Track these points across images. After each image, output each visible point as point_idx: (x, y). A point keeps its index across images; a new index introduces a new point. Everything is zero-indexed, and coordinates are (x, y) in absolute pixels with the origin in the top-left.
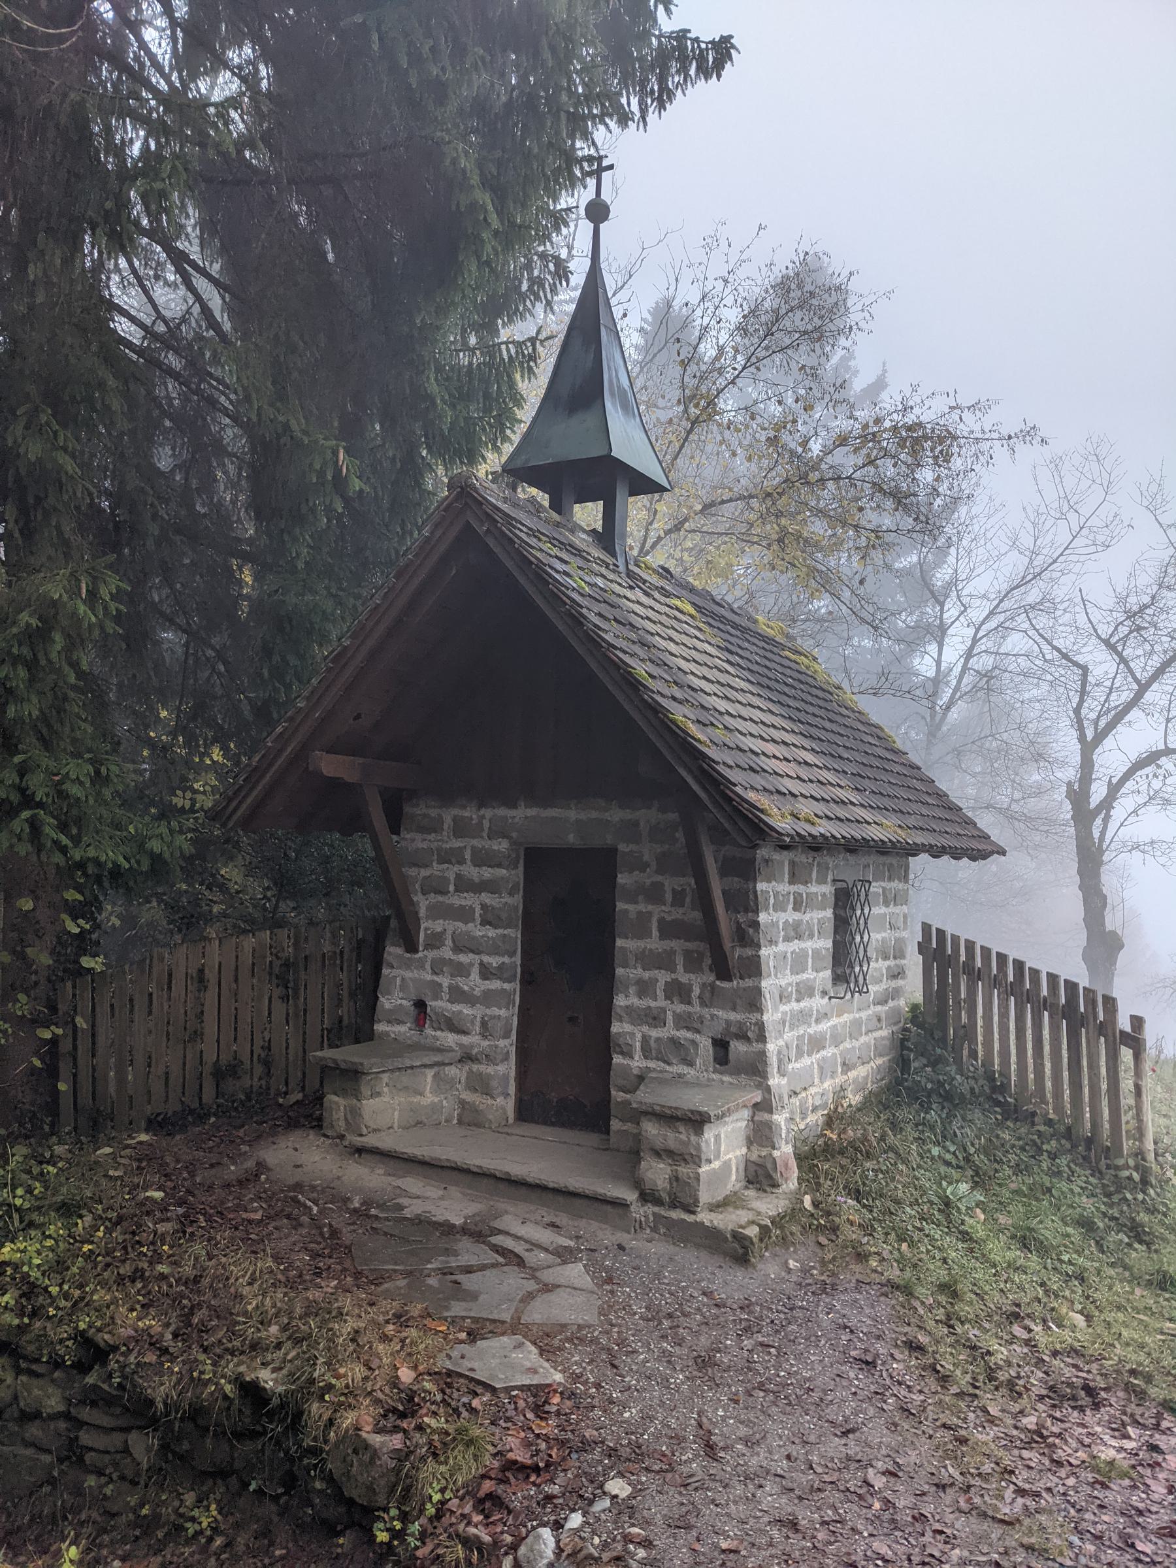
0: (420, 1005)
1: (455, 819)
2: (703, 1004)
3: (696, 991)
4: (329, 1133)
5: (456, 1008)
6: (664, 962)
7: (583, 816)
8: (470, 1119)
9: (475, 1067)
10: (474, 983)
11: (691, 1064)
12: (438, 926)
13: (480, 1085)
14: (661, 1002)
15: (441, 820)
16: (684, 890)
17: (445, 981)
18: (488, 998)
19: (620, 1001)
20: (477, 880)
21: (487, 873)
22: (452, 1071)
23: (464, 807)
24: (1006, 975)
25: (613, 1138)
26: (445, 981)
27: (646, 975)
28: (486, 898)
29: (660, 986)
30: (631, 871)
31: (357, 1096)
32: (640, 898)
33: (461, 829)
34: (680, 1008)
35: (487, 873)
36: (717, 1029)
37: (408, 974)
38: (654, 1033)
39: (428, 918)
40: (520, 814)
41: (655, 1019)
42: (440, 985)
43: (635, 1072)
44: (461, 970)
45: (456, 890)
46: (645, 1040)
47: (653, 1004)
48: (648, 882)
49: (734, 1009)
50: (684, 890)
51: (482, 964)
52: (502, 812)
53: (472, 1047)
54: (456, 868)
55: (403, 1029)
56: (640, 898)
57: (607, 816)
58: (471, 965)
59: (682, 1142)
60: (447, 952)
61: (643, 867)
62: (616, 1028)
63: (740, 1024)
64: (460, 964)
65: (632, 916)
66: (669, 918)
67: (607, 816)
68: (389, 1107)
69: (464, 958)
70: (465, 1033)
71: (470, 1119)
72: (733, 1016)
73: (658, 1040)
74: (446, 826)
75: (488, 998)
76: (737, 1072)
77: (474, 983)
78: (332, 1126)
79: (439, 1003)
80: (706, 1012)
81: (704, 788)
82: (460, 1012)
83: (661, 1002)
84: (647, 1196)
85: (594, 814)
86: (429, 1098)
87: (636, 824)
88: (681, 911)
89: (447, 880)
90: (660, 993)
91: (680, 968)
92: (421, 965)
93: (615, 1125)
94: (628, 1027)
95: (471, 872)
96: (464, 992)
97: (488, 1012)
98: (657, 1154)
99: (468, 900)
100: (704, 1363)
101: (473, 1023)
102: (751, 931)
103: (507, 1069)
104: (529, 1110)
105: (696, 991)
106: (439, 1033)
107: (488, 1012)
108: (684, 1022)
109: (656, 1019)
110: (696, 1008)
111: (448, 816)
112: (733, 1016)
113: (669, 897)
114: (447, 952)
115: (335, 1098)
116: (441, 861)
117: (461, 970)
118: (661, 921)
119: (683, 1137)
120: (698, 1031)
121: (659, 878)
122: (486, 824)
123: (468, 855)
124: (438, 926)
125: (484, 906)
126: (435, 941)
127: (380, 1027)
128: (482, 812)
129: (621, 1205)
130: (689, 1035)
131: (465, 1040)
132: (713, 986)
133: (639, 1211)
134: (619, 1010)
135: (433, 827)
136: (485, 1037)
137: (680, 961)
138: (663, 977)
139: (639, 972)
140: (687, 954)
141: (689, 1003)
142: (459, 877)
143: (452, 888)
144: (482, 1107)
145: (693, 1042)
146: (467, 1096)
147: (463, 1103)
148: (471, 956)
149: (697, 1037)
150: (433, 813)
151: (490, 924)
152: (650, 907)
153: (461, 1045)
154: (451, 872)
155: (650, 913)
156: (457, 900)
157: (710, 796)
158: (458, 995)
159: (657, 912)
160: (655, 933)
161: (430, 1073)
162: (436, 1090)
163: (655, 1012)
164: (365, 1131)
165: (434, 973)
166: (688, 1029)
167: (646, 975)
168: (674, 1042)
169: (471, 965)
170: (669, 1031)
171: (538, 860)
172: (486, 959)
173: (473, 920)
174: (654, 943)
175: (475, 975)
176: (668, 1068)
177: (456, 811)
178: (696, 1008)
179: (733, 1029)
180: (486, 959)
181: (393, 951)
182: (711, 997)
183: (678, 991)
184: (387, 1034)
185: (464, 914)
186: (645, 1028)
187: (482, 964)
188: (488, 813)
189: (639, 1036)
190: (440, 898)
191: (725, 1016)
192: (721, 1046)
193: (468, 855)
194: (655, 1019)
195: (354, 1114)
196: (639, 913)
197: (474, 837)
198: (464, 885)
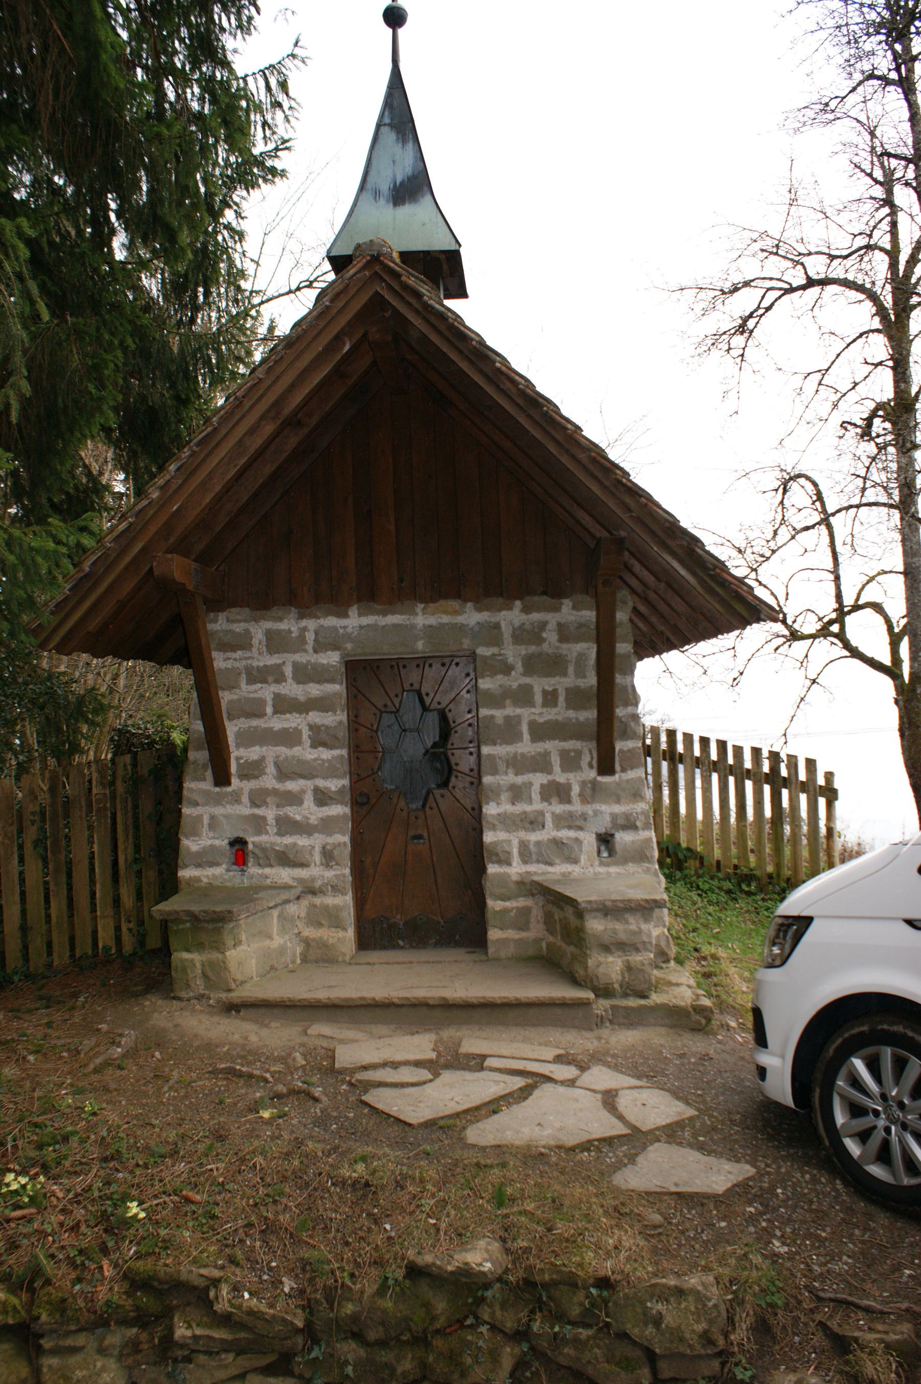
0: (239, 844)
1: (269, 634)
2: (584, 799)
3: (576, 790)
4: (183, 994)
5: (288, 840)
6: (541, 764)
7: (432, 620)
8: (317, 956)
9: (318, 901)
10: (310, 811)
11: (576, 861)
12: (254, 753)
13: (316, 918)
14: (537, 805)
15: (247, 634)
16: (555, 690)
17: (270, 813)
18: (326, 826)
19: (490, 810)
20: (302, 699)
21: (314, 690)
22: (292, 909)
23: (280, 619)
24: (654, 763)
25: (491, 950)
26: (270, 813)
27: (519, 780)
28: (315, 717)
29: (536, 788)
30: (493, 675)
31: (219, 947)
32: (508, 702)
33: (275, 643)
34: (559, 808)
35: (314, 690)
36: (602, 825)
37: (218, 811)
38: (533, 837)
39: (238, 746)
40: (354, 621)
41: (532, 823)
42: (264, 818)
43: (515, 878)
44: (295, 799)
45: (275, 712)
46: (523, 845)
47: (528, 808)
48: (515, 685)
49: (618, 801)
50: (555, 690)
51: (317, 790)
52: (330, 621)
53: (313, 879)
54: (274, 688)
55: (218, 871)
56: (508, 702)
57: (460, 619)
58: (303, 792)
59: (634, 933)
60: (269, 781)
61: (507, 669)
62: (489, 837)
63: (627, 816)
64: (289, 792)
65: (499, 721)
66: (541, 720)
67: (460, 619)
68: (256, 954)
69: (292, 786)
70: (303, 865)
71: (317, 956)
72: (618, 809)
73: (538, 843)
74: (255, 642)
75: (326, 826)
76: (625, 861)
77: (310, 811)
78: (188, 986)
79: (263, 838)
80: (589, 809)
81: (694, 574)
82: (295, 844)
83: (537, 805)
84: (604, 992)
85: (446, 619)
86: (278, 941)
87: (497, 626)
88: (555, 710)
89: (263, 702)
90: (536, 796)
91: (557, 768)
92: (236, 798)
93: (494, 934)
94: (502, 835)
95: (291, 689)
96: (297, 822)
97: (330, 840)
98: (606, 949)
99: (292, 721)
100: (320, 1174)
101: (311, 855)
102: (632, 724)
103: (346, 901)
104: (374, 934)
105: (576, 790)
106: (267, 871)
107: (330, 840)
108: (562, 821)
109: (534, 822)
110: (577, 807)
111: (258, 631)
112: (618, 809)
113: (538, 698)
114: (269, 781)
115: (186, 955)
116: (251, 681)
117: (295, 799)
118: (533, 725)
119: (633, 927)
120: (580, 828)
121: (527, 680)
122: (310, 637)
123: (288, 671)
124: (254, 753)
125: (311, 727)
126: (252, 770)
127: (185, 874)
128: (304, 623)
129: (583, 1004)
130: (572, 834)
131: (303, 873)
132: (594, 783)
133: (602, 1006)
134: (490, 819)
135: (242, 643)
136: (327, 866)
137: (556, 760)
138: (538, 780)
139: (510, 778)
140: (564, 754)
141: (569, 801)
142: (277, 697)
143: (269, 710)
144: (331, 941)
145: (577, 839)
146: (309, 932)
147: (307, 942)
148: (302, 782)
149: (580, 835)
150: (239, 628)
151: (325, 745)
152: (518, 711)
153: (301, 881)
154: (267, 692)
155: (519, 717)
156: (277, 723)
157: (702, 582)
158: (287, 826)
159: (526, 714)
160: (526, 736)
161: (275, 913)
162: (283, 931)
163: (532, 816)
164: (233, 986)
165: (254, 804)
166: (570, 827)
167: (519, 780)
168: (558, 844)
169: (303, 792)
170: (549, 833)
171: (363, 673)
172: (321, 783)
173: (300, 743)
174: (526, 747)
175: (309, 801)
176: (550, 869)
177: (269, 625)
178: (577, 807)
179: (620, 821)
180: (321, 783)
181: (197, 786)
182: (592, 792)
183: (560, 792)
184: (198, 880)
185: (289, 738)
186: (522, 834)
187: (317, 790)
188: (311, 624)
189: (515, 843)
190: (255, 722)
191: (609, 811)
192: (605, 840)
193: (288, 671)
194: (532, 823)
195: (220, 967)
196: (507, 719)
197: (294, 652)
198: (283, 705)
